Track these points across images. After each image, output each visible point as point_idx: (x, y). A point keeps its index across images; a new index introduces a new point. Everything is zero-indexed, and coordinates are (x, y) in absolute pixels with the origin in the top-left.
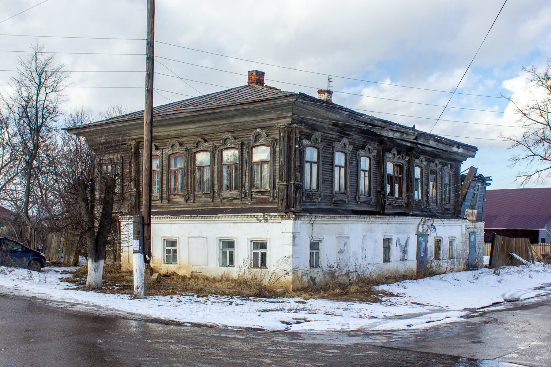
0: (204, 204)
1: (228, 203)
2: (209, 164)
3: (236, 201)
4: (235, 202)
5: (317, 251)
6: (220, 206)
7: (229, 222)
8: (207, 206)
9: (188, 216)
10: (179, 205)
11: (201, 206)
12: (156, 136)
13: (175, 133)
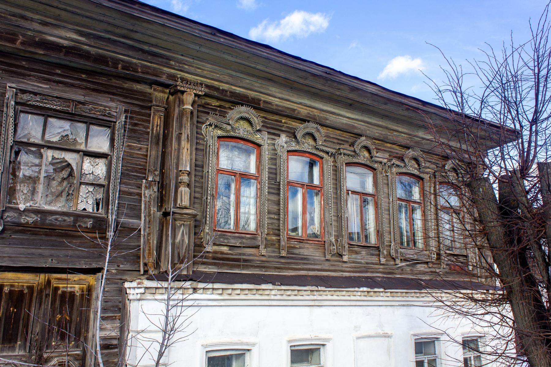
0: (365, 267)
1: (408, 269)
2: (42, 119)
3: (421, 267)
4: (421, 267)
5: (431, 357)
6: (395, 274)
7: (381, 303)
8: (372, 272)
9: (365, 289)
10: (311, 264)
11: (358, 270)
12: (260, 100)
13: (306, 111)
